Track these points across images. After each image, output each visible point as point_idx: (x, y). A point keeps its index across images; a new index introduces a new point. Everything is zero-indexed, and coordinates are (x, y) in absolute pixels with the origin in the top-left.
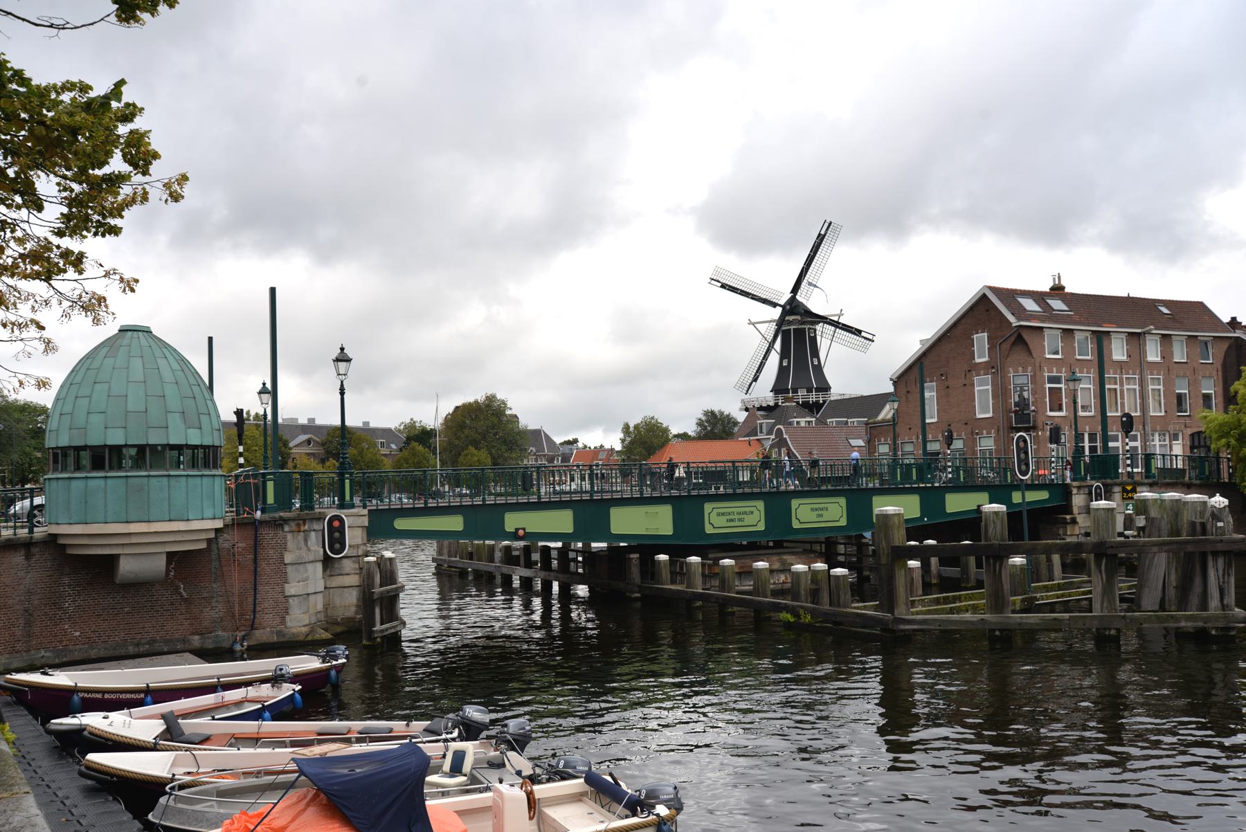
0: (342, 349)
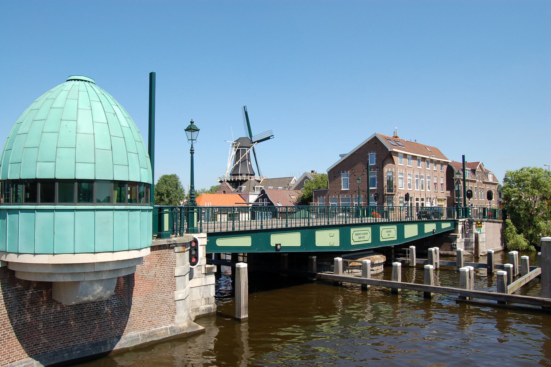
0: (192, 122)
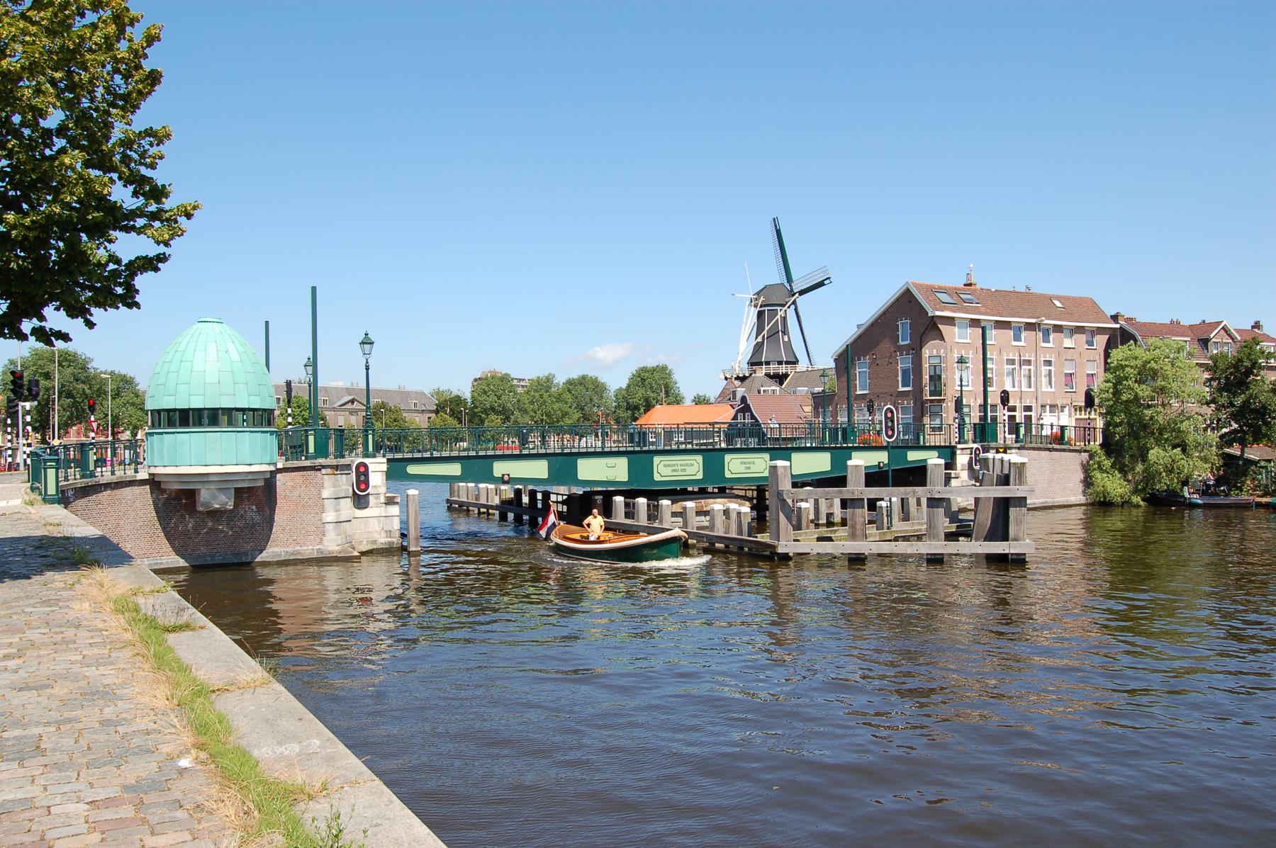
0: (366, 334)
